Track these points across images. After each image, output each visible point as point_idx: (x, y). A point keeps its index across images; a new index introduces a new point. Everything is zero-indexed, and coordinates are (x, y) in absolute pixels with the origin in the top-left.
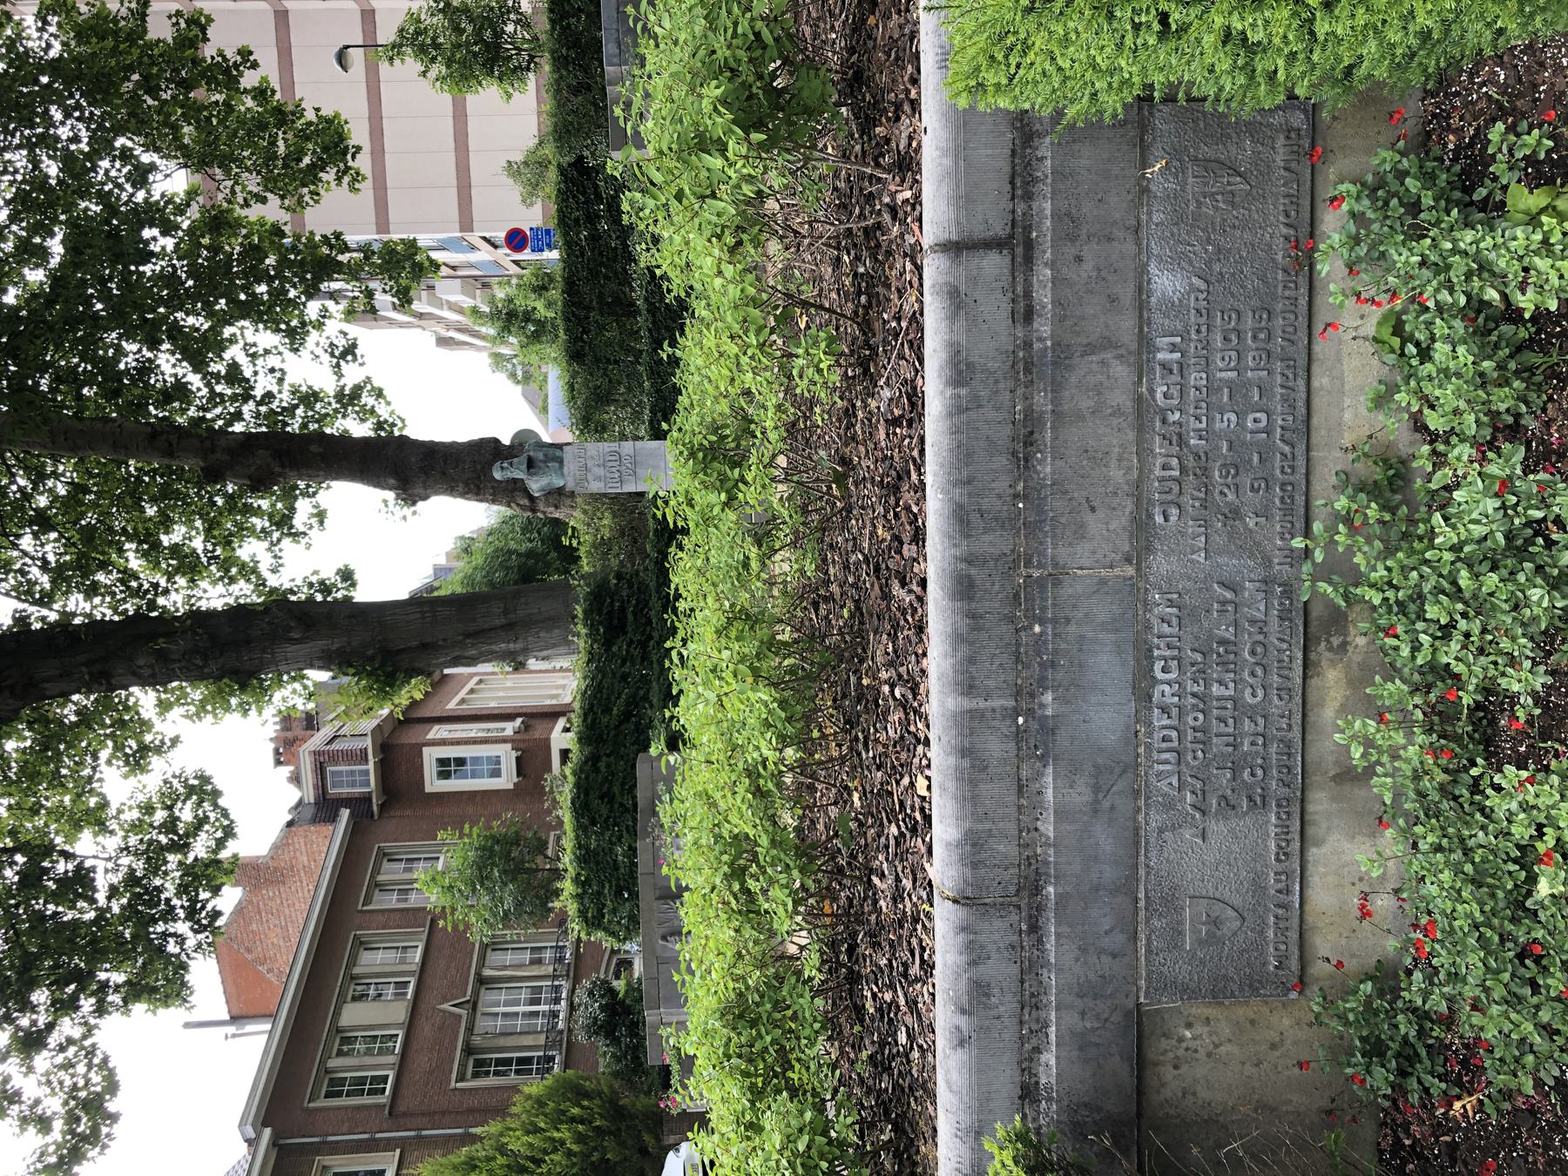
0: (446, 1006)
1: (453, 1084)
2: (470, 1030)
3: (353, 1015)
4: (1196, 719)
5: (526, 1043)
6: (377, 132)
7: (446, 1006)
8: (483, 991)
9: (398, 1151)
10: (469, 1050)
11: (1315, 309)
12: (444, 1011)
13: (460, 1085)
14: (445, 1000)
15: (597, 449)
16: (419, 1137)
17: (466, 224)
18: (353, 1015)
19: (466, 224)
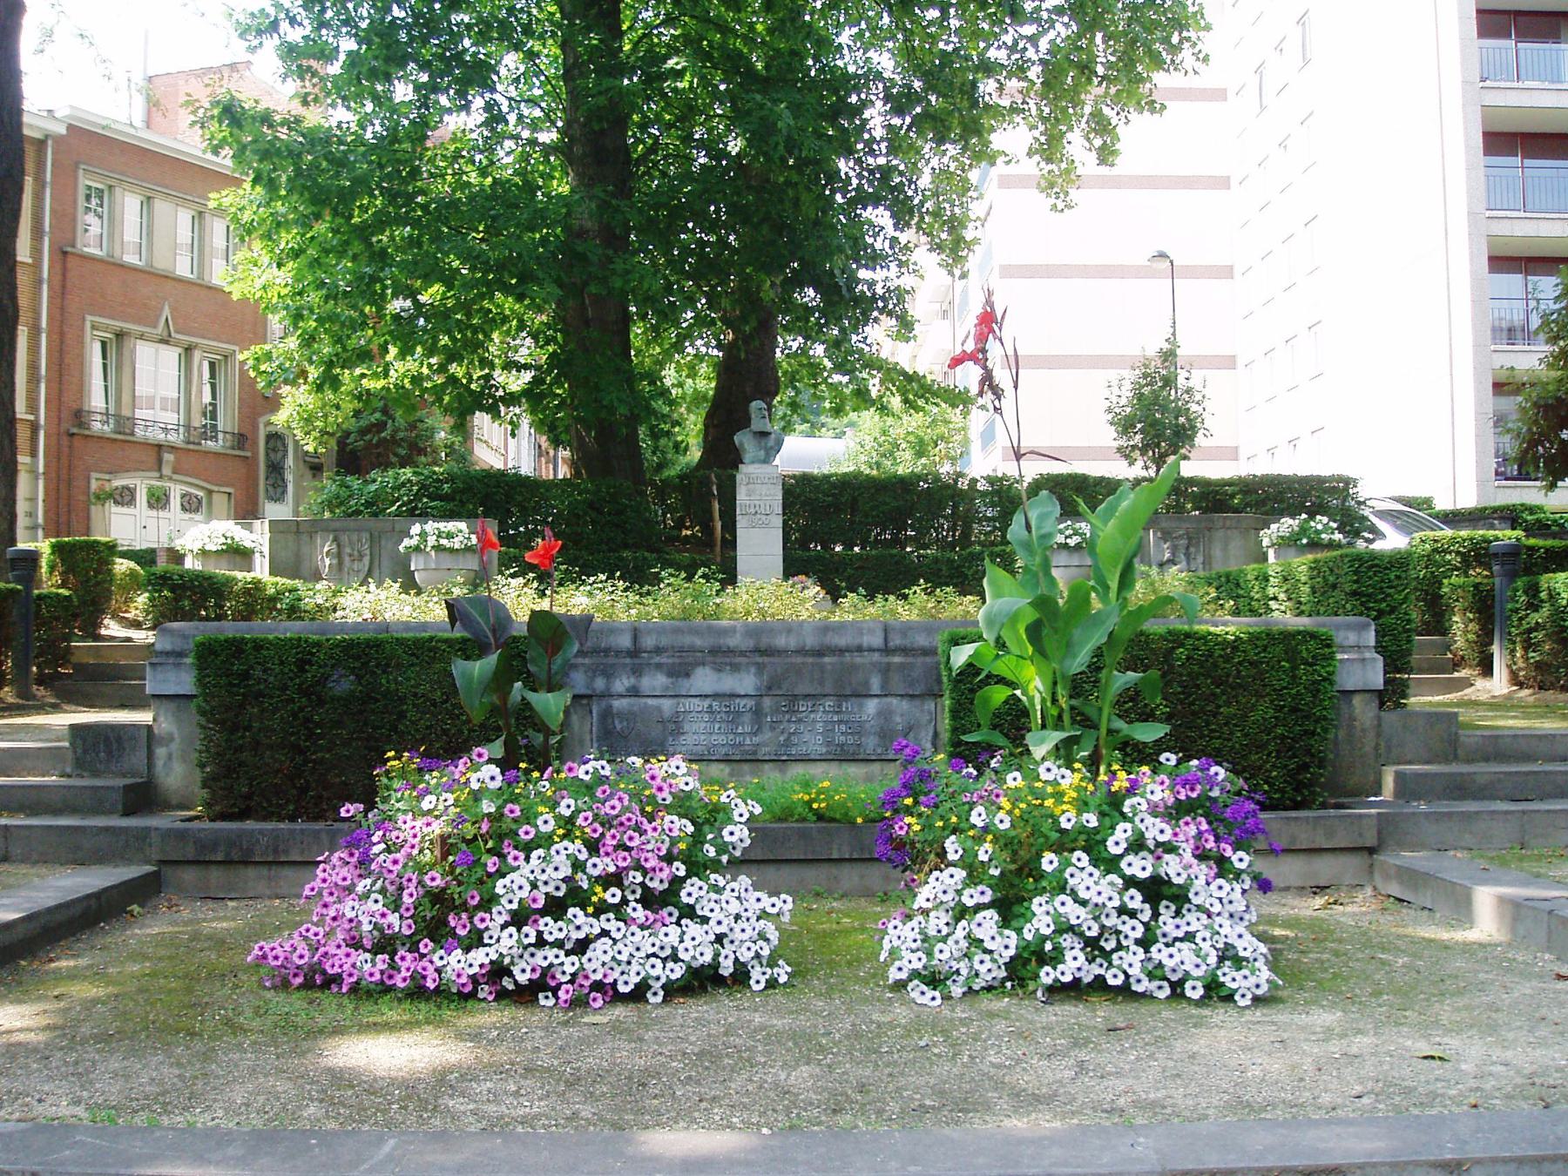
0: (167, 312)
1: (89, 318)
2: (142, 337)
3: (130, 205)
4: (473, 897)
5: (124, 395)
6: (1003, 318)
7: (167, 312)
8: (179, 350)
9: (30, 261)
10: (120, 336)
11: (869, 864)
12: (162, 309)
13: (88, 325)
14: (173, 310)
15: (774, 499)
16: (40, 282)
17: (1008, 271)
18: (130, 205)
19: (1008, 271)
